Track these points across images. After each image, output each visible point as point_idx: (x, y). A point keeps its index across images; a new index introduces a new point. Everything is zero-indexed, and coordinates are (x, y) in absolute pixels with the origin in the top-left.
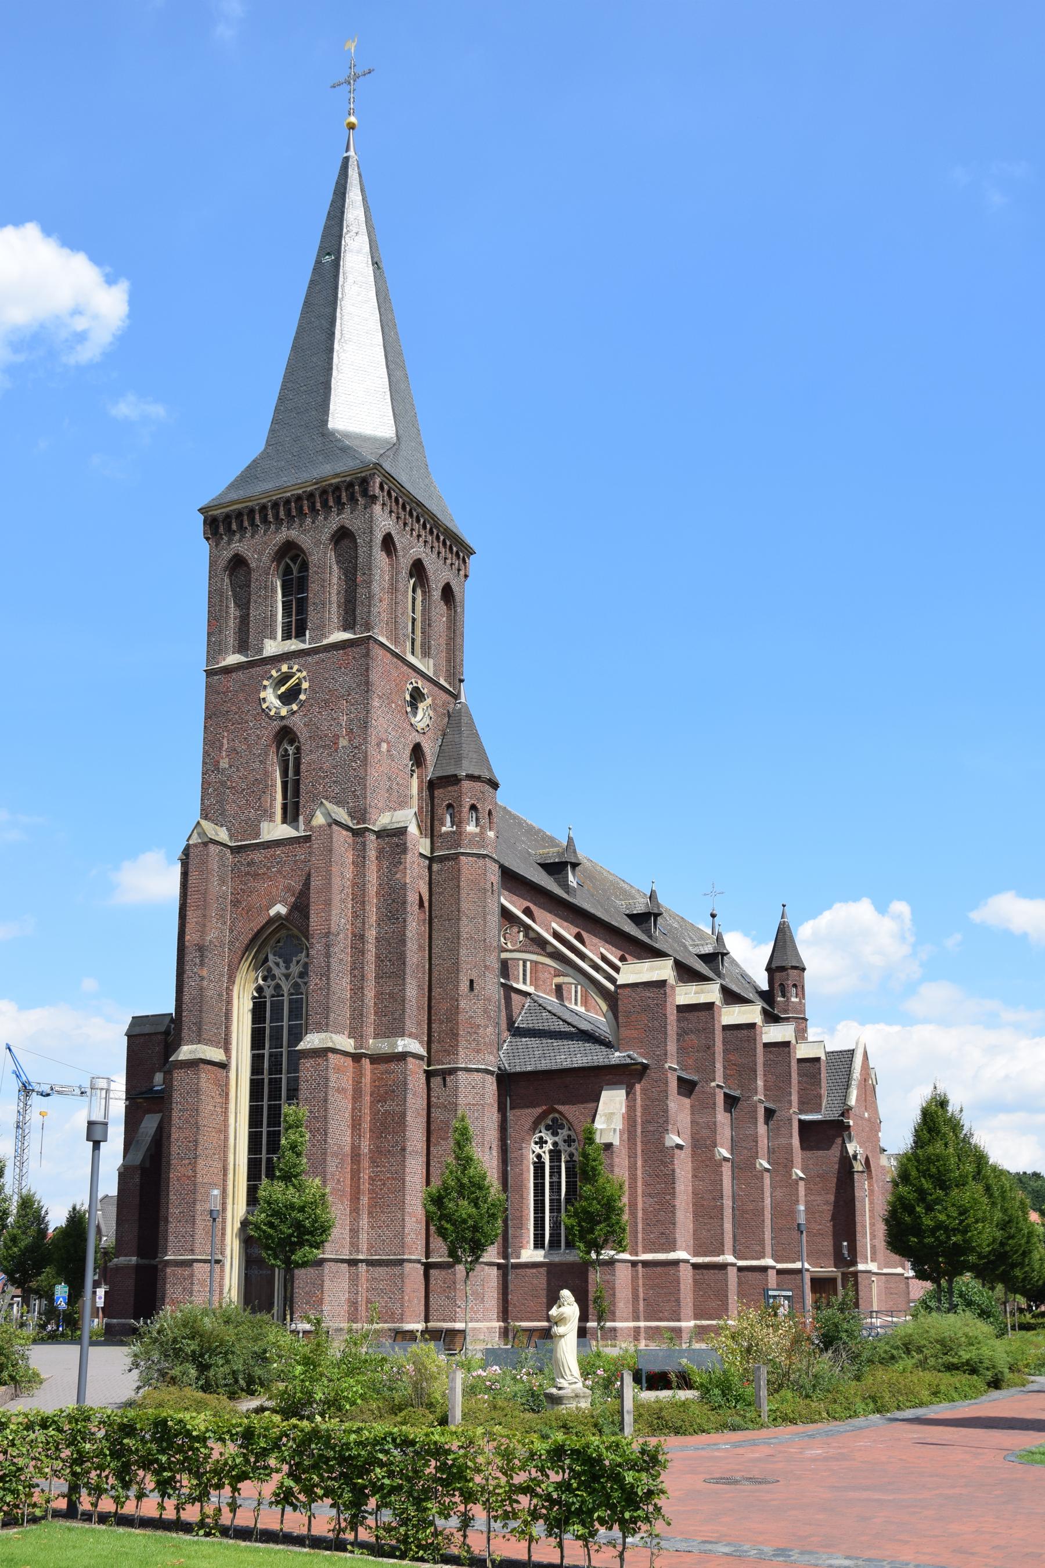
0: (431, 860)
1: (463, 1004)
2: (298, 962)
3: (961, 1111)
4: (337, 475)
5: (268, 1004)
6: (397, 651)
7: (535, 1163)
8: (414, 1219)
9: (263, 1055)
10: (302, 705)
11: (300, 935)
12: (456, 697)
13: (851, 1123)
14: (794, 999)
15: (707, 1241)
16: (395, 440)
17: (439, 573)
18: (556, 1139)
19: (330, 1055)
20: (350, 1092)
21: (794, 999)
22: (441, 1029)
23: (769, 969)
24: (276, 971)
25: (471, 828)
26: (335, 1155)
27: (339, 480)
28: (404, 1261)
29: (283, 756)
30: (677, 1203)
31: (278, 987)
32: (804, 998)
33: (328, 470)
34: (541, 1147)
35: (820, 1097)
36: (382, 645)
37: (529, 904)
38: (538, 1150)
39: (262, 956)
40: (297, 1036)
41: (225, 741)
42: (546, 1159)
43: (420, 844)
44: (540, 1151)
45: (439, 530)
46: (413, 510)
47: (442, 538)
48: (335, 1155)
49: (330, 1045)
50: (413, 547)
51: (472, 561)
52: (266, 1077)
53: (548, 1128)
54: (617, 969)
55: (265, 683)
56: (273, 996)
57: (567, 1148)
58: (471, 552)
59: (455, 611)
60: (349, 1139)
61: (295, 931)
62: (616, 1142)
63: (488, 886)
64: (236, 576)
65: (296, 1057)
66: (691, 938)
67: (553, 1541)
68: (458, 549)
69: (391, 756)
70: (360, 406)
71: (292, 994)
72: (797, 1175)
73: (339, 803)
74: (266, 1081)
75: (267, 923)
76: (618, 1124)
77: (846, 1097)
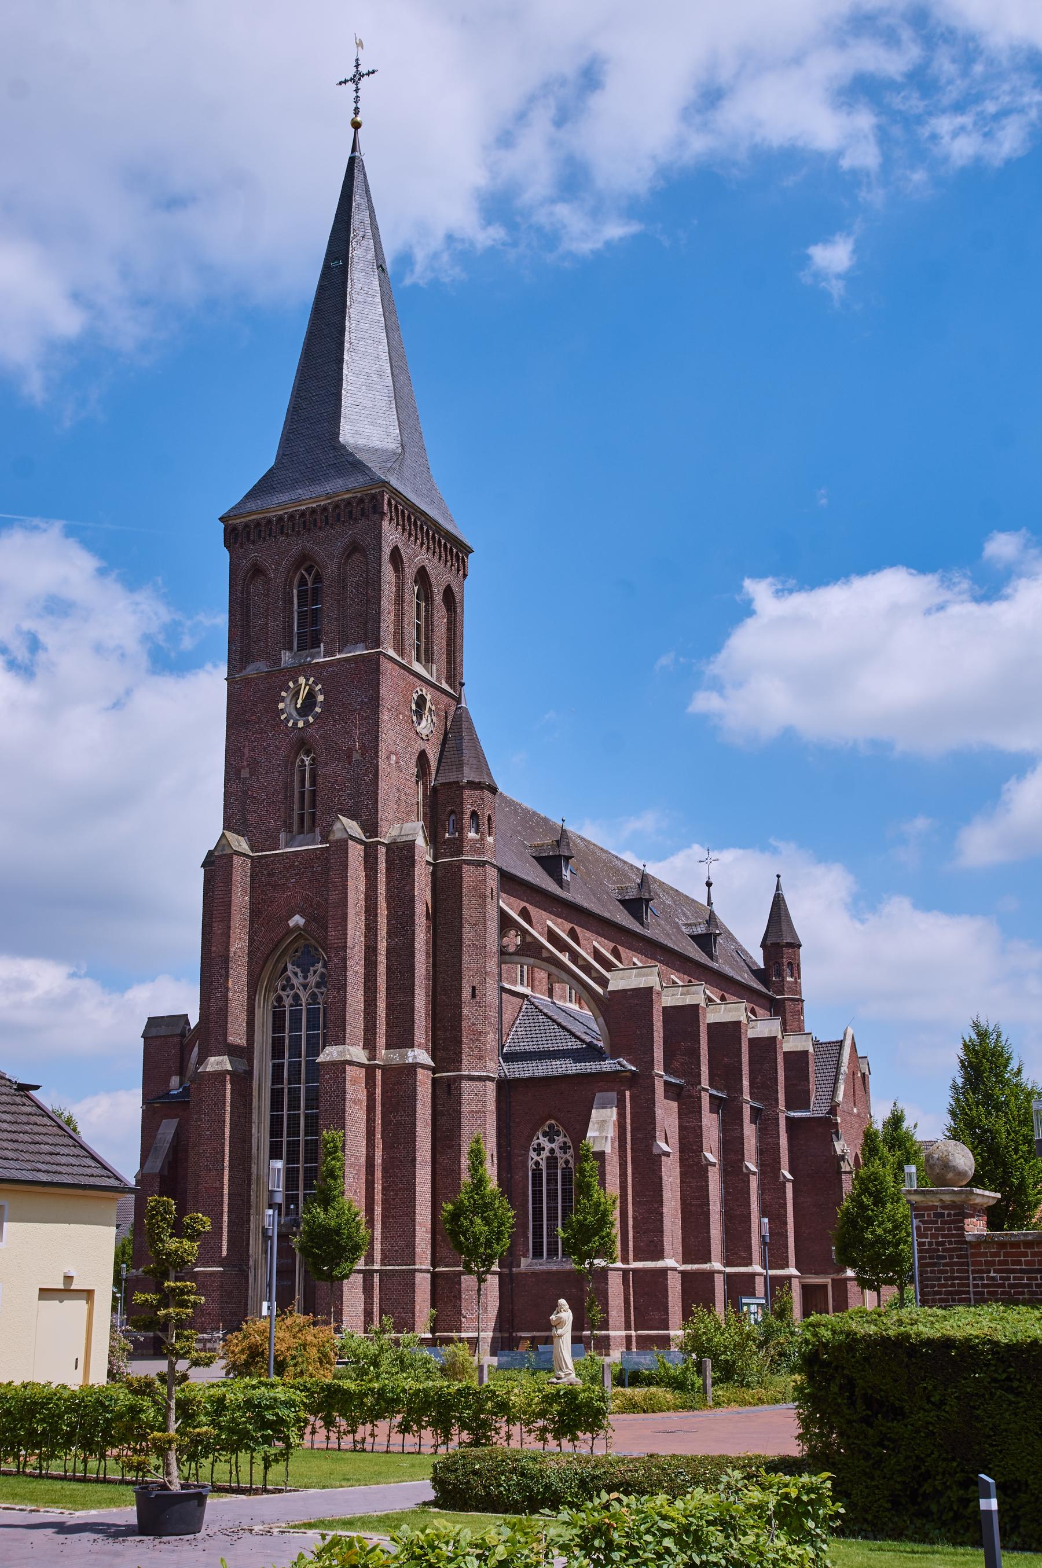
0: (435, 866)
1: (466, 1011)
2: (315, 972)
3: (915, 1126)
4: (348, 491)
5: (287, 1013)
6: (403, 662)
7: (533, 1170)
8: (424, 1229)
9: (283, 1065)
10: (317, 717)
11: (317, 945)
12: (458, 700)
13: (839, 1121)
14: (789, 979)
15: (695, 1247)
16: (400, 450)
17: (440, 576)
18: (553, 1146)
19: (348, 1067)
20: (365, 1103)
21: (789, 979)
22: (447, 1045)
23: (763, 945)
24: (295, 981)
25: (472, 835)
26: (352, 1166)
27: (350, 495)
28: (415, 1270)
29: (300, 766)
30: (665, 1210)
31: (296, 997)
32: (799, 977)
33: (338, 487)
34: (539, 1155)
35: (808, 1092)
36: (391, 659)
37: (523, 904)
38: (536, 1158)
39: (281, 966)
40: (314, 1049)
41: (246, 750)
42: (543, 1165)
43: (423, 851)
44: (539, 1159)
45: (440, 535)
46: (419, 524)
47: (443, 541)
48: (352, 1166)
49: (348, 1057)
50: (416, 556)
51: (471, 560)
52: (286, 1086)
53: (545, 1135)
54: (608, 966)
55: (283, 694)
56: (292, 1006)
57: (562, 1155)
58: (468, 551)
59: (455, 612)
60: (364, 1150)
61: (313, 942)
62: (608, 1150)
63: (488, 892)
64: (254, 585)
65: (315, 1069)
66: (684, 914)
67: (556, 1442)
68: (455, 551)
69: (399, 768)
70: (366, 422)
71: (310, 1004)
72: (784, 1176)
73: (352, 817)
74: (286, 1090)
75: (286, 934)
76: (611, 1132)
77: (834, 1092)
